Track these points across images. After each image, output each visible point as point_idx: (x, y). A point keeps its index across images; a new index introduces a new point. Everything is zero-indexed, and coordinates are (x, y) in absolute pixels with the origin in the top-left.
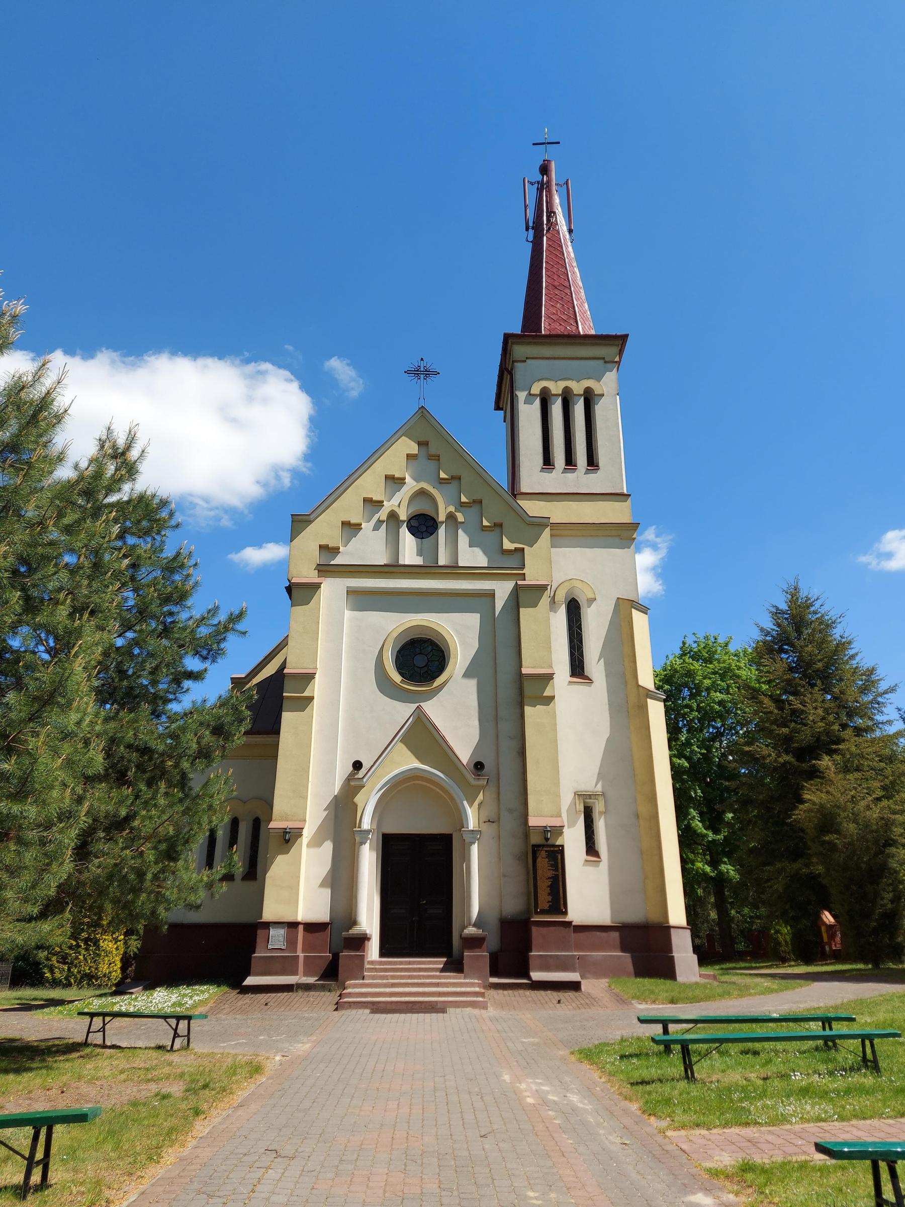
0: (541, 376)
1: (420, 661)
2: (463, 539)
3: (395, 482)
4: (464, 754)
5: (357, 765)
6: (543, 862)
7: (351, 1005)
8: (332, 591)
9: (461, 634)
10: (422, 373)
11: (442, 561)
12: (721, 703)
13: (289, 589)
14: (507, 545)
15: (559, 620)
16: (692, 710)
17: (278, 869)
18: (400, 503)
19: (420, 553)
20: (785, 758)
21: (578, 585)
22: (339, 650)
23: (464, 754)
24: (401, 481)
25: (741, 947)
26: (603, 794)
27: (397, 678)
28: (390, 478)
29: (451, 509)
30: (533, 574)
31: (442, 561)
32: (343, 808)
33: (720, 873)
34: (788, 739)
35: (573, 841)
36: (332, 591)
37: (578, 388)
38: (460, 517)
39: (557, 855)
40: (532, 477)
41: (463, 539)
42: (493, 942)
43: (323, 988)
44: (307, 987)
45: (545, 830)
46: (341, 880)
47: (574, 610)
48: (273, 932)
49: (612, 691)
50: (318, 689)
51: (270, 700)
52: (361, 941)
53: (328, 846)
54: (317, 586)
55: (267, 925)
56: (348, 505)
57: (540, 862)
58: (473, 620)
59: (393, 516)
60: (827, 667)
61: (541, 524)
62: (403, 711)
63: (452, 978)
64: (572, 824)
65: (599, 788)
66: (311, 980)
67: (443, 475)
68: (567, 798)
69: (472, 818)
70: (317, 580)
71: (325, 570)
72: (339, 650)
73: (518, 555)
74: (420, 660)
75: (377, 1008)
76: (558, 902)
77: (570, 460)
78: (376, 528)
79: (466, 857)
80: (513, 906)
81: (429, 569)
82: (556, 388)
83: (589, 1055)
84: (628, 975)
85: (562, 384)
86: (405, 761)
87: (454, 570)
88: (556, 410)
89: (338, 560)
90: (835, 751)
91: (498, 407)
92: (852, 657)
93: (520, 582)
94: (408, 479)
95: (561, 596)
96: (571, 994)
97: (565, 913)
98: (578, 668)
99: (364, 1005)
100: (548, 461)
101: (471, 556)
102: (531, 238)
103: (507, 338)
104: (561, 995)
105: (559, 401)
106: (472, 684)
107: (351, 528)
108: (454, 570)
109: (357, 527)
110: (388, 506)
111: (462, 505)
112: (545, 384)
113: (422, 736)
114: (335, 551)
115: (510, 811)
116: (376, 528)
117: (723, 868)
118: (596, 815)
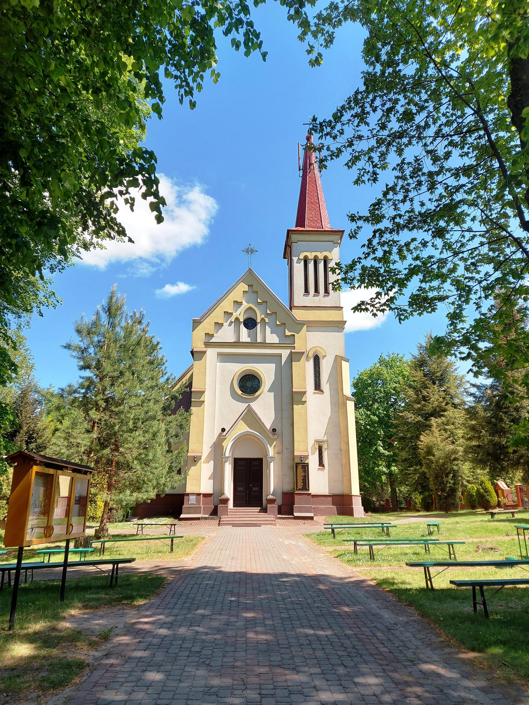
0: (305, 250)
1: (249, 384)
2: (268, 329)
3: (238, 304)
4: (268, 425)
5: (223, 430)
6: (300, 469)
7: (225, 524)
8: (211, 353)
9: (267, 372)
10: (250, 251)
11: (259, 340)
12: (394, 389)
13: (192, 353)
14: (288, 333)
15: (310, 365)
16: (381, 392)
17: (192, 471)
18: (240, 314)
19: (249, 336)
20: (419, 418)
21: (319, 349)
22: (215, 379)
23: (268, 425)
24: (241, 303)
25: (403, 506)
26: (327, 441)
27: (240, 392)
28: (235, 302)
29: (263, 316)
30: (299, 347)
31: (259, 340)
32: (218, 447)
33: (391, 471)
34: (420, 409)
35: (313, 461)
36: (211, 353)
37: (321, 256)
38: (267, 320)
39: (305, 467)
40: (299, 299)
41: (268, 329)
42: (279, 502)
43: (212, 519)
44: (206, 518)
45: (301, 457)
46: (217, 476)
47: (317, 360)
48: (191, 497)
49: (332, 397)
50: (207, 397)
51: (185, 400)
52: (226, 501)
53: (212, 462)
54: (205, 352)
55: (188, 494)
56: (217, 315)
57: (300, 468)
58: (272, 367)
59: (237, 319)
60: (442, 375)
61: (302, 324)
62: (242, 407)
63: (263, 515)
64: (313, 454)
65: (325, 438)
66: (207, 516)
67: (259, 301)
68: (311, 443)
69: (271, 451)
70: (204, 349)
71: (208, 344)
72: (215, 379)
73: (292, 337)
74: (249, 384)
75: (234, 525)
76: (306, 485)
77: (317, 290)
78: (230, 325)
79: (268, 467)
80: (288, 487)
81: (253, 344)
82: (311, 256)
83: (308, 536)
84: (335, 515)
85: (314, 254)
86: (243, 428)
87: (264, 345)
88: (311, 266)
89: (213, 340)
90: (443, 415)
91: (285, 257)
92: (456, 370)
93: (293, 351)
94: (244, 303)
95: (311, 354)
96: (310, 521)
97: (309, 490)
98: (318, 386)
99: (230, 524)
100: (307, 290)
101: (272, 338)
102: (301, 175)
103: (289, 231)
104: (305, 521)
105: (312, 262)
106: (272, 394)
107: (219, 325)
108: (264, 345)
109: (222, 325)
110: (235, 315)
111: (268, 314)
112: (306, 254)
113: (250, 417)
114: (212, 336)
115: (287, 449)
116: (230, 325)
117: (393, 468)
118: (323, 450)
